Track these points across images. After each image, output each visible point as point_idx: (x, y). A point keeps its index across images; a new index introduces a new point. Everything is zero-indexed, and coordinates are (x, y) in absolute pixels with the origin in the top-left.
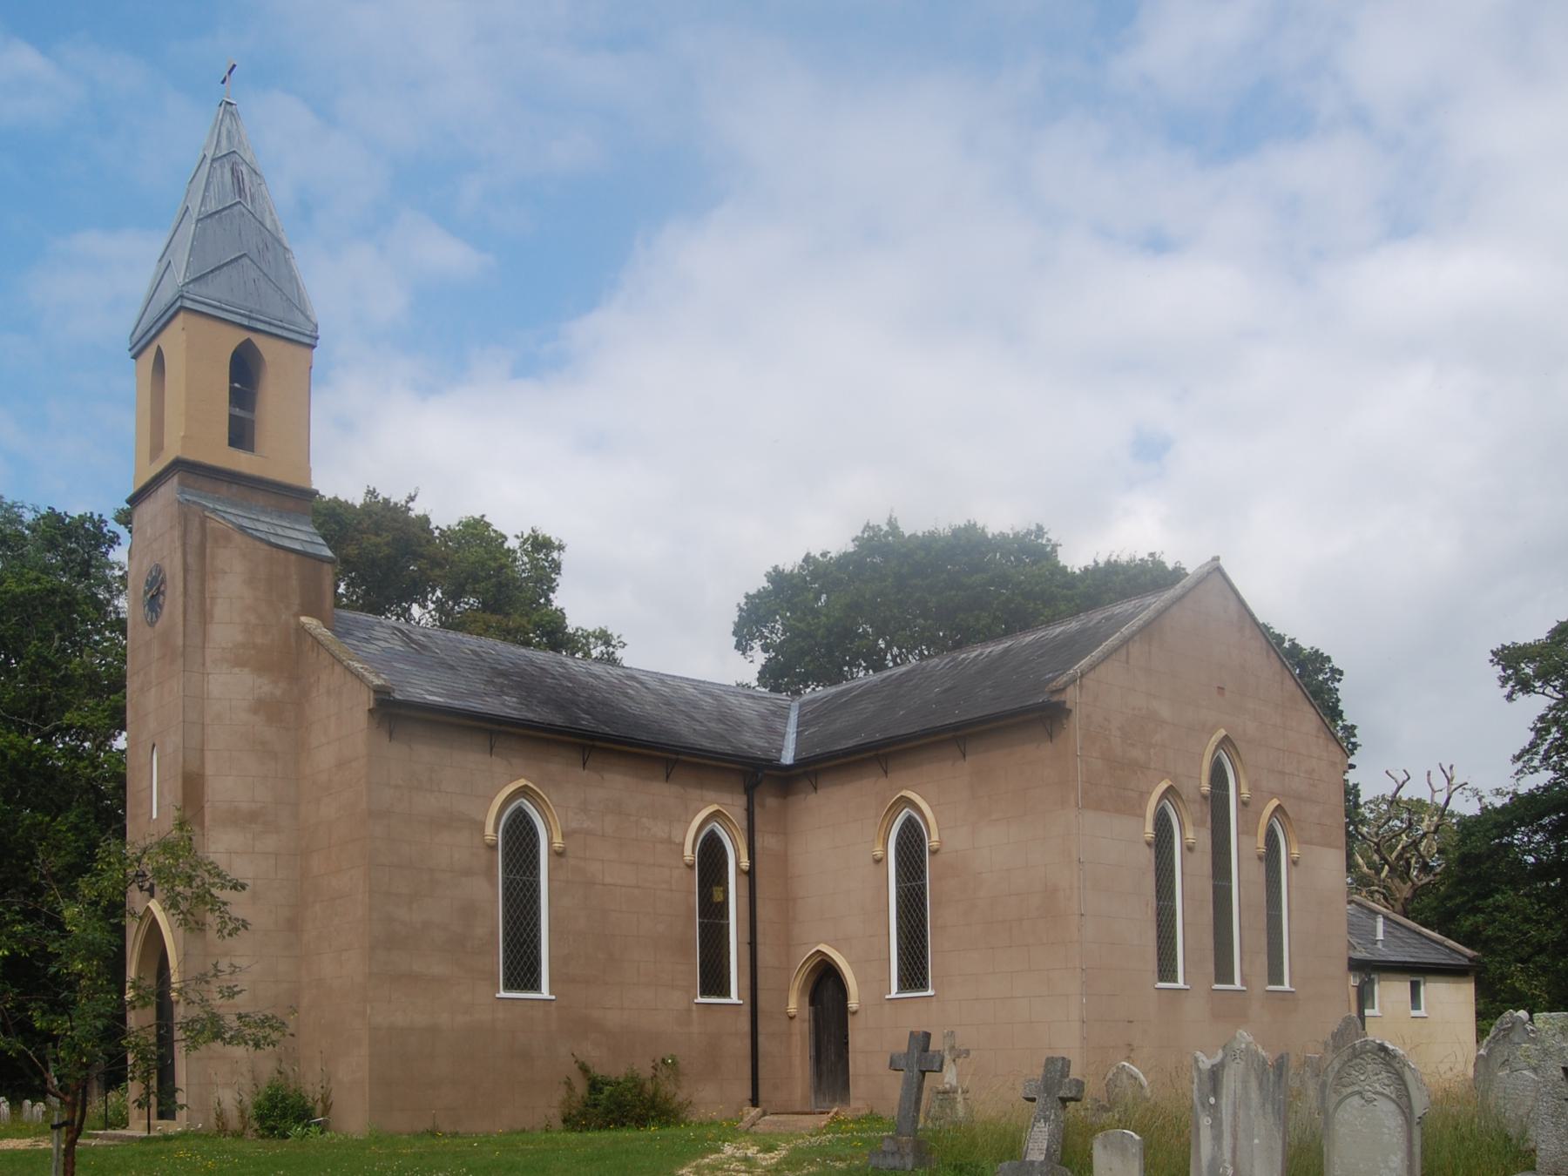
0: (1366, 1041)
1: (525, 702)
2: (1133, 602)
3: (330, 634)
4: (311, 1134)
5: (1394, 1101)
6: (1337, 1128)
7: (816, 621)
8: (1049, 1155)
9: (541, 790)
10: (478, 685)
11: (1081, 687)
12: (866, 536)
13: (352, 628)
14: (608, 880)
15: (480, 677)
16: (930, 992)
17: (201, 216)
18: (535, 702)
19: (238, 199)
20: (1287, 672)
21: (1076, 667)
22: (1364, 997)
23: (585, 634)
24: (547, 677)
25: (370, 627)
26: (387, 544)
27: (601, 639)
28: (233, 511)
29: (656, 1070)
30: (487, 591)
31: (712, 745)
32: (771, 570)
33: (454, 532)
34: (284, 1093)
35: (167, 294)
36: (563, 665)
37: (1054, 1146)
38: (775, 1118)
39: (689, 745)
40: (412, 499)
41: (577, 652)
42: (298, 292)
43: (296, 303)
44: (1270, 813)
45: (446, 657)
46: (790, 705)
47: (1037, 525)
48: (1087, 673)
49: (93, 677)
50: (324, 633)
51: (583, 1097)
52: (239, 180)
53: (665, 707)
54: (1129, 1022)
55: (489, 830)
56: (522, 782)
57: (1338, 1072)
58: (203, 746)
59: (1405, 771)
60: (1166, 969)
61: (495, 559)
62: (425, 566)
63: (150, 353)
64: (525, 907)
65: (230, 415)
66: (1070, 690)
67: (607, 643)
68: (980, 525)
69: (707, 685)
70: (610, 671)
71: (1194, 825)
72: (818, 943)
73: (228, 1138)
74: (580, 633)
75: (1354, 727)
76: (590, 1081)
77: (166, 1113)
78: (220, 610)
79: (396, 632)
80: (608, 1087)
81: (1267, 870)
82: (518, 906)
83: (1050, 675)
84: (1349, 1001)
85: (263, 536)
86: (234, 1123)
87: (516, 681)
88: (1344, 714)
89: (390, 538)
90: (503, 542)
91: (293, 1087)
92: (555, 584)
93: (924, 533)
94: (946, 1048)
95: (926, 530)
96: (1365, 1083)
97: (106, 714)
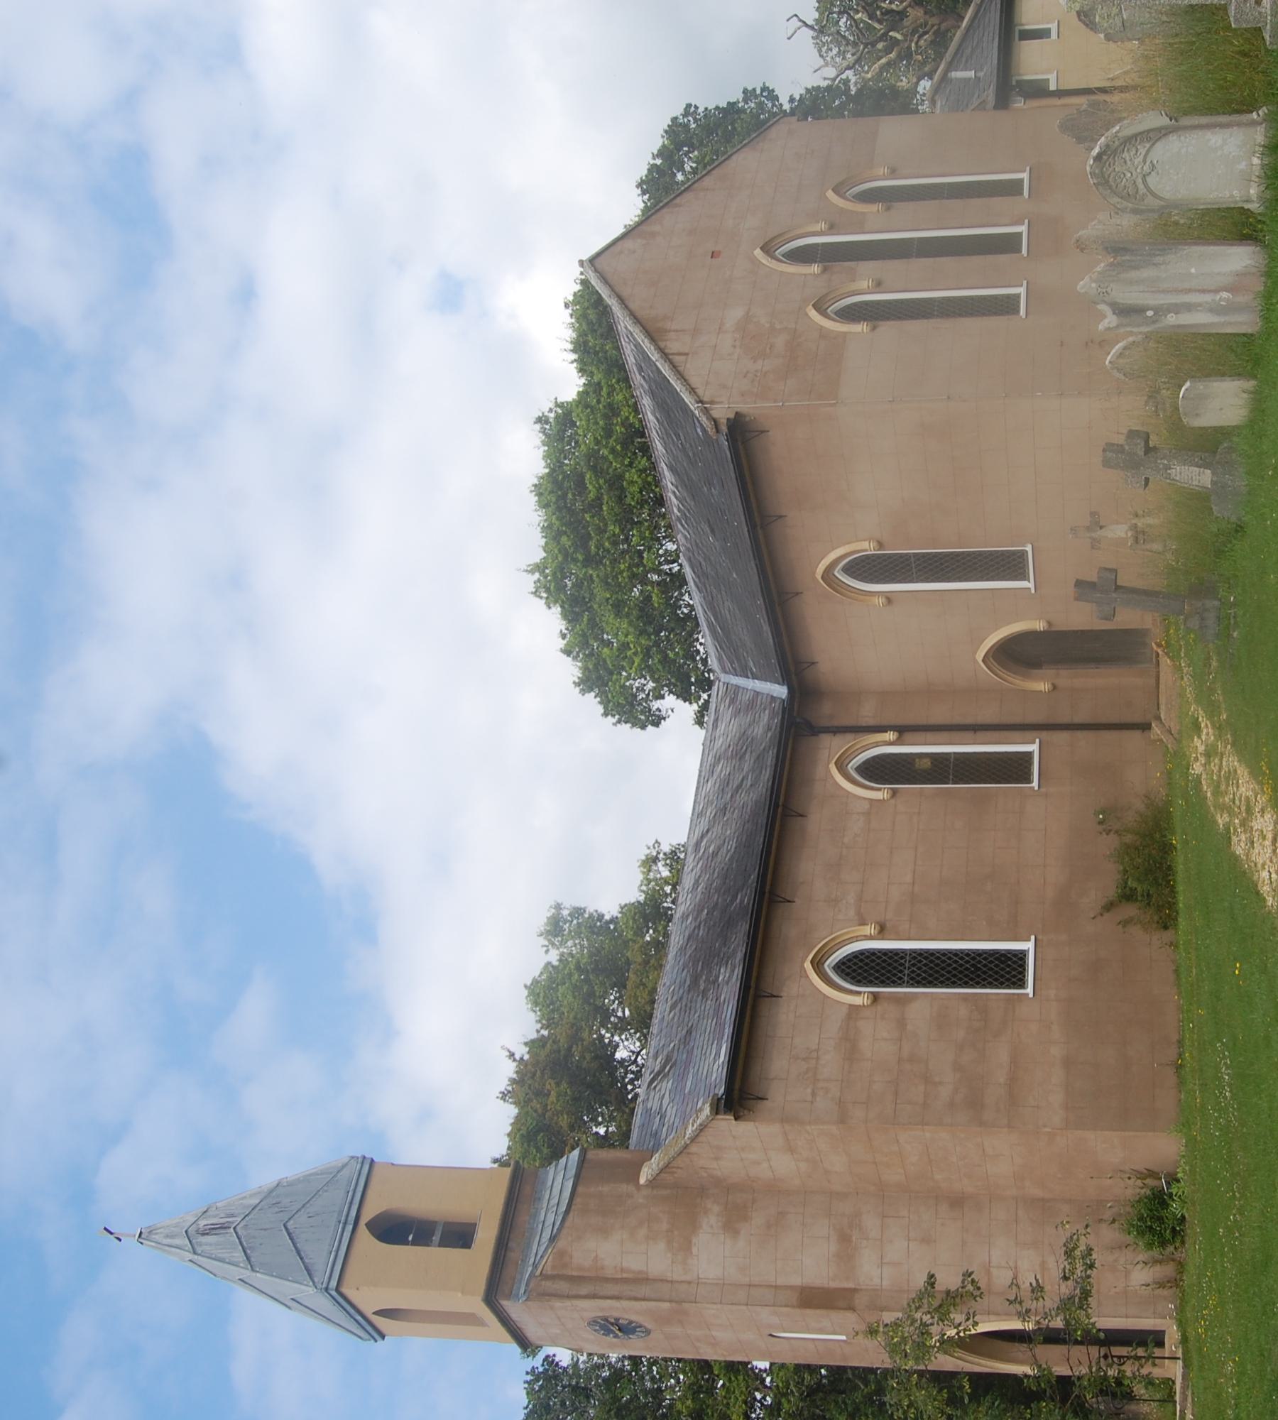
0: (1091, 173)
1: (725, 959)
2: (623, 343)
3: (657, 1155)
4: (1180, 1193)
5: (1153, 144)
6: (1180, 197)
7: (632, 646)
8: (1205, 465)
9: (815, 946)
10: (708, 1007)
11: (712, 402)
12: (545, 595)
13: (649, 1131)
14: (909, 878)
15: (698, 1005)
16: (1029, 548)
17: (249, 1267)
18: (724, 949)
19: (232, 1230)
20: (696, 185)
21: (691, 407)
22: (1038, 90)
23: (645, 882)
24: (698, 934)
25: (648, 1112)
26: (558, 1084)
27: (650, 866)
28: (535, 1247)
29: (1110, 831)
30: (603, 984)
31: (768, 770)
32: (578, 689)
33: (543, 1017)
34: (1135, 1218)
35: (324, 1303)
36: (685, 917)
37: (1196, 460)
38: (1162, 707)
39: (769, 793)
40: (512, 1055)
41: (663, 890)
42: (318, 1174)
43: (330, 1177)
44: (839, 199)
45: (678, 1038)
46: (724, 683)
47: (535, 423)
48: (698, 397)
49: (694, 1390)
50: (656, 1162)
51: (1140, 909)
52: (213, 1229)
53: (728, 815)
54: (1062, 345)
55: (857, 1000)
56: (808, 965)
57: (1122, 198)
58: (772, 1286)
59: (788, 20)
60: (1006, 306)
61: (570, 975)
62: (580, 1047)
63: (380, 1322)
64: (937, 965)
65: (440, 1246)
66: (715, 414)
67: (655, 860)
68: (536, 481)
69: (704, 768)
70: (691, 867)
71: (854, 281)
72: (975, 661)
73: (1185, 1278)
74: (644, 888)
75: (745, 91)
76: (1124, 900)
77: (1158, 1339)
78: (635, 1263)
79: (654, 1085)
80: (1129, 883)
81: (902, 201)
82: (937, 972)
83: (699, 430)
84: (1040, 107)
85: (560, 1218)
86: (1168, 1270)
87: (702, 966)
88: (731, 101)
89: (552, 1082)
90: (553, 966)
91: (1129, 1209)
92: (595, 914)
93: (543, 537)
94: (1088, 535)
95: (540, 535)
96: (1134, 173)
97: (733, 1379)
